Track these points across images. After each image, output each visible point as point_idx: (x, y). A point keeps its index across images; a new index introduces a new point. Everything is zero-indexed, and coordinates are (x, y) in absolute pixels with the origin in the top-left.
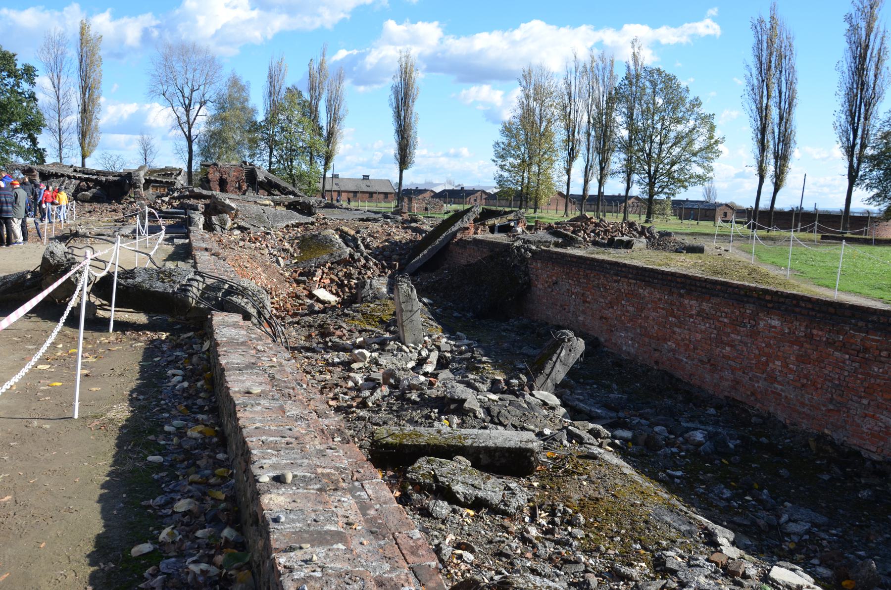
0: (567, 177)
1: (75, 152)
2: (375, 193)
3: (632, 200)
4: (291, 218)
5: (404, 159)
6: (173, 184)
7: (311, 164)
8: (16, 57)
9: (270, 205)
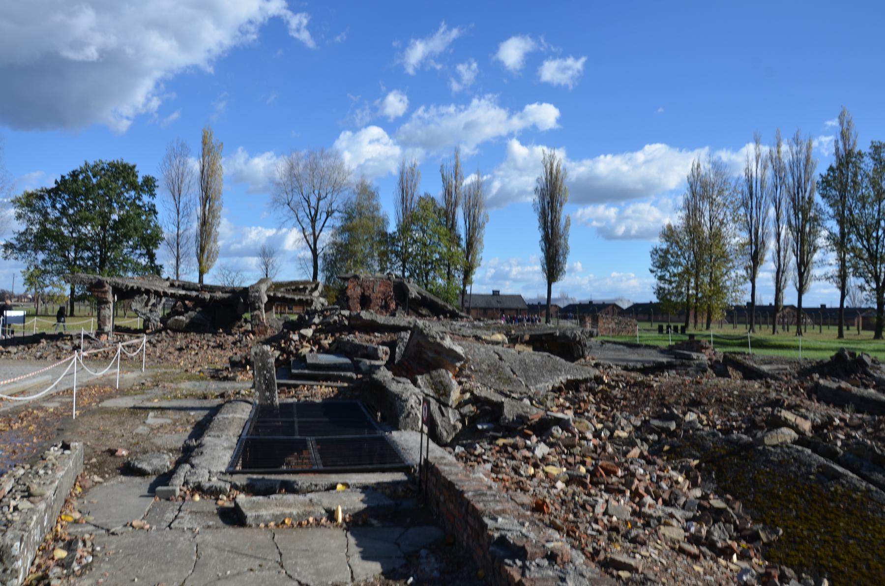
1: (193, 268)
3: (787, 310)
5: (553, 268)
6: (309, 303)
7: (449, 278)
8: (136, 169)
9: (503, 343)
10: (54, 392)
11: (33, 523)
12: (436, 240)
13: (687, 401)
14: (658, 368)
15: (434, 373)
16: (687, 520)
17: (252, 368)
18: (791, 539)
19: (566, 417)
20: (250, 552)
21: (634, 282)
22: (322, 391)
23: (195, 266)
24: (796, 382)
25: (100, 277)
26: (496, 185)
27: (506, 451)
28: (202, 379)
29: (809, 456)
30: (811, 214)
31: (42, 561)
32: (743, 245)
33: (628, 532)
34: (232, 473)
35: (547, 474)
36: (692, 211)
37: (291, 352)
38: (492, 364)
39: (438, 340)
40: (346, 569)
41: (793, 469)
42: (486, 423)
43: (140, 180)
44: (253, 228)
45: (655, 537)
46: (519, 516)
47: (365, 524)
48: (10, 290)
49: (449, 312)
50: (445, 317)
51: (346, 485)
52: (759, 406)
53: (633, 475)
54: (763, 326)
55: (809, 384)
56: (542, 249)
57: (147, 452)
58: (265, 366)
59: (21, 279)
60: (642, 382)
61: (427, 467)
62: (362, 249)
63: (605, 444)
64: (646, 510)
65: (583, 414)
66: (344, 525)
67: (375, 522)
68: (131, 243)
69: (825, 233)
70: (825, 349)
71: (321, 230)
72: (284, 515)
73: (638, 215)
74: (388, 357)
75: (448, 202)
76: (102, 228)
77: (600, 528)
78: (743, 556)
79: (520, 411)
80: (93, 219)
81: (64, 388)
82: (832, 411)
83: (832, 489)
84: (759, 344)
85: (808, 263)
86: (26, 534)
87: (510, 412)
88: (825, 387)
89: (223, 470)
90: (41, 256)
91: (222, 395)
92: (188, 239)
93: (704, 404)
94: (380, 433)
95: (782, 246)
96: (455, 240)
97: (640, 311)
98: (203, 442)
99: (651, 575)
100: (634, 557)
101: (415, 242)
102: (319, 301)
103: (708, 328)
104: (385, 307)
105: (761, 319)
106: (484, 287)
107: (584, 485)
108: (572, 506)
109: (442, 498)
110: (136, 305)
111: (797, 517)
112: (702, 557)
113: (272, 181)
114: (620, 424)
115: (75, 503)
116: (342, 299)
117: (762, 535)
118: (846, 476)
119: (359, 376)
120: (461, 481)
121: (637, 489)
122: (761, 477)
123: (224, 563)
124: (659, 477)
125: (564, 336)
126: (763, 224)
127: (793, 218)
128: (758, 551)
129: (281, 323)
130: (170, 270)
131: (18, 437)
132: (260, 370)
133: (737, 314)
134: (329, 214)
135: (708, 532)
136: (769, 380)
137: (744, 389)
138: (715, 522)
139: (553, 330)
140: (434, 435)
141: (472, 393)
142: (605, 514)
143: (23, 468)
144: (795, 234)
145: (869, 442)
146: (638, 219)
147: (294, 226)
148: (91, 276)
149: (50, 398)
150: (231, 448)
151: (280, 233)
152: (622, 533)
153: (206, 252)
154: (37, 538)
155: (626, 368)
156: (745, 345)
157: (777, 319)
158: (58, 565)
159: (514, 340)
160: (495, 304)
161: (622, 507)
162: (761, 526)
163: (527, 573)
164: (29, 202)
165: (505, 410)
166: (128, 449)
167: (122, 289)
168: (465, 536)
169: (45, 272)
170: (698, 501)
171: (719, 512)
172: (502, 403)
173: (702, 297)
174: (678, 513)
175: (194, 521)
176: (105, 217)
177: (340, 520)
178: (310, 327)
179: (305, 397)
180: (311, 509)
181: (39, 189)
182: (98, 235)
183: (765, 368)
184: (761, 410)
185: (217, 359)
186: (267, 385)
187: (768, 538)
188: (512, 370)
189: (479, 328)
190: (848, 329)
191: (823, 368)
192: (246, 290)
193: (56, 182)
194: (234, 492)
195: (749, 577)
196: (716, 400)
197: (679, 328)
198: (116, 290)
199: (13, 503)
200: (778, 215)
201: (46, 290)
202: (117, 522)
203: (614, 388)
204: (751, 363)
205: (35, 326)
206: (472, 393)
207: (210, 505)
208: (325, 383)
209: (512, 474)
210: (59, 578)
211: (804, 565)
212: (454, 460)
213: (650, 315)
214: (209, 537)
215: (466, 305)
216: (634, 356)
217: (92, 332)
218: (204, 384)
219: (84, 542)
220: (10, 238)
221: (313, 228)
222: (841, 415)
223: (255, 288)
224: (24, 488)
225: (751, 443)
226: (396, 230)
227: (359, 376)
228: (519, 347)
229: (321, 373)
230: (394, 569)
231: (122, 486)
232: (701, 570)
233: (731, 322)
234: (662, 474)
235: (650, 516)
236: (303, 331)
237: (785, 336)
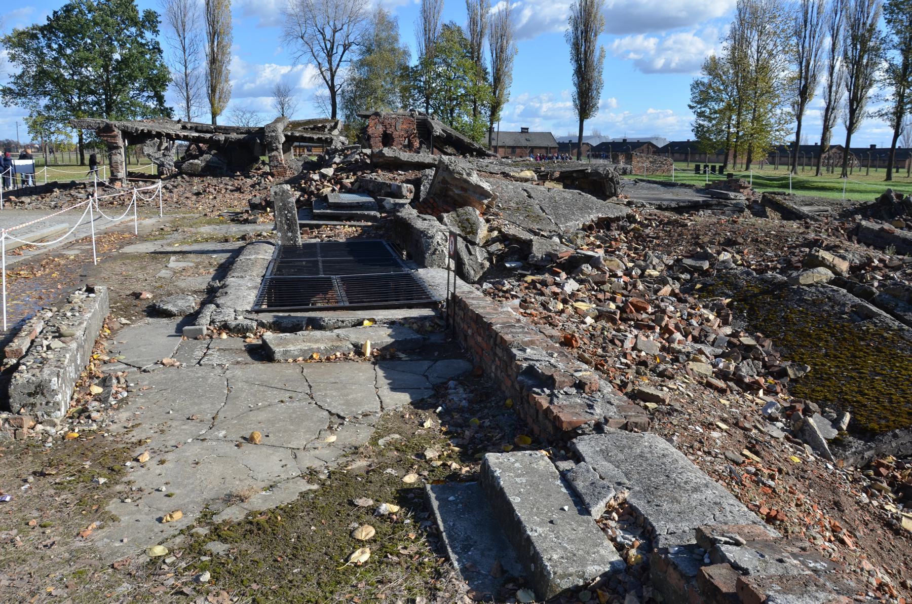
0: (797, 123)
1: (205, 110)
2: (519, 147)
3: (834, 150)
4: (585, 209)
5: (585, 104)
6: (329, 142)
7: (475, 115)
9: (532, 180)
10: (73, 239)
11: (67, 361)
12: (461, 73)
13: (722, 240)
14: (694, 207)
15: (460, 210)
16: (716, 357)
17: (272, 207)
18: (819, 376)
19: (597, 255)
20: (280, 385)
21: (671, 120)
22: (345, 231)
23: (207, 108)
24: (837, 223)
25: (108, 121)
26: (527, 13)
27: (535, 288)
28: (222, 222)
29: (844, 295)
30: (871, 44)
31: (80, 396)
32: (792, 79)
33: (657, 366)
34: (257, 312)
35: (576, 309)
36: (739, 41)
37: (312, 192)
38: (520, 202)
39: (465, 176)
40: (375, 400)
41: (826, 308)
42: (514, 259)
43: (141, 15)
44: (267, 65)
45: (684, 372)
46: (548, 347)
47: (393, 358)
48: (15, 140)
49: (475, 150)
50: (472, 155)
51: (373, 321)
52: (797, 246)
53: (664, 312)
54: (806, 168)
55: (850, 225)
56: (575, 84)
57: (172, 294)
58: (285, 206)
59: (25, 127)
60: (676, 221)
61: (455, 301)
62: (381, 83)
63: (636, 281)
64: (675, 345)
65: (613, 252)
66: (373, 359)
67: (403, 356)
68: (137, 85)
69: (885, 65)
70: (870, 192)
71: (338, 65)
72: (311, 350)
73: (679, 46)
74: (412, 194)
75: (473, 32)
76: (104, 70)
77: (629, 362)
78: (769, 391)
79: (550, 249)
80: (94, 59)
81: (83, 235)
82: (872, 252)
83: (864, 328)
84: (800, 186)
85: (861, 99)
86: (62, 371)
87: (539, 250)
88: (867, 228)
89: (249, 309)
90: (44, 101)
91: (243, 238)
92: (197, 78)
93: (740, 244)
94: (406, 270)
95: (835, 80)
96: (481, 74)
97: (678, 150)
98: (227, 283)
99: (677, 406)
100: (662, 390)
101: (439, 75)
102: (339, 140)
103: (747, 169)
104: (409, 147)
105: (805, 160)
106: (513, 125)
107: (614, 321)
108: (601, 340)
109: (470, 332)
110: (149, 148)
111: (826, 355)
112: (729, 392)
113: (284, 12)
114: (651, 263)
115: (106, 344)
116: (364, 138)
117: (790, 371)
118: (880, 315)
119: (383, 215)
120: (489, 313)
121: (667, 325)
122: (793, 315)
123: (255, 395)
124: (690, 314)
125: (596, 173)
126: (816, 55)
127: (850, 49)
128: (784, 386)
129: (301, 163)
130: (181, 113)
131: (43, 284)
132: (281, 209)
133: (778, 154)
134: (346, 47)
135: (737, 368)
136: (808, 220)
137: (782, 229)
138: (744, 358)
139: (586, 168)
140: (460, 272)
141: (500, 232)
142: (633, 349)
143: (51, 310)
144: (851, 66)
145: (907, 283)
146: (679, 51)
147: (309, 62)
148: (98, 120)
149: (70, 245)
150: (255, 288)
151: (295, 69)
152: (650, 367)
153: (218, 92)
154: (73, 375)
155: (659, 207)
156: (786, 186)
157: (822, 160)
158: (95, 400)
159: (543, 177)
160: (524, 143)
161: (651, 343)
162: (790, 363)
163: (555, 400)
164: (21, 41)
165: (534, 248)
166: (152, 292)
167: (131, 133)
168: (493, 367)
169: (50, 119)
170: (728, 338)
171: (749, 348)
172: (531, 241)
173: (744, 135)
174: (708, 350)
175: (225, 354)
176: (107, 57)
177: (368, 354)
178: (330, 166)
179: (329, 237)
180: (339, 344)
181: (30, 26)
182: (101, 76)
183: (805, 209)
184: (798, 250)
185: (236, 203)
186: (288, 225)
187: (795, 374)
188: (541, 208)
189: (508, 165)
190: (897, 172)
191: (866, 210)
192: (262, 129)
193: (48, 19)
194: (262, 330)
195: (773, 410)
196: (752, 241)
197: (717, 168)
198: (126, 134)
199: (45, 343)
200: (834, 44)
201: (53, 138)
202: (148, 361)
203: (647, 226)
204: (791, 204)
205: (44, 176)
206: (500, 232)
207: (238, 343)
208: (348, 223)
209: (541, 309)
210: (98, 411)
211: (829, 400)
212: (482, 295)
213: (687, 154)
214: (238, 372)
215: (494, 143)
216: (669, 195)
217: (105, 179)
218: (224, 227)
219: (118, 378)
220: (6, 82)
221: (330, 62)
222: (881, 257)
223: (272, 127)
224: (54, 329)
225: (786, 282)
226: (417, 63)
227: (383, 215)
228: (548, 184)
229: (343, 213)
230: (423, 400)
231: (149, 327)
232: (727, 403)
233: (772, 163)
234: (693, 312)
235: (679, 352)
236: (323, 171)
237: (828, 177)
